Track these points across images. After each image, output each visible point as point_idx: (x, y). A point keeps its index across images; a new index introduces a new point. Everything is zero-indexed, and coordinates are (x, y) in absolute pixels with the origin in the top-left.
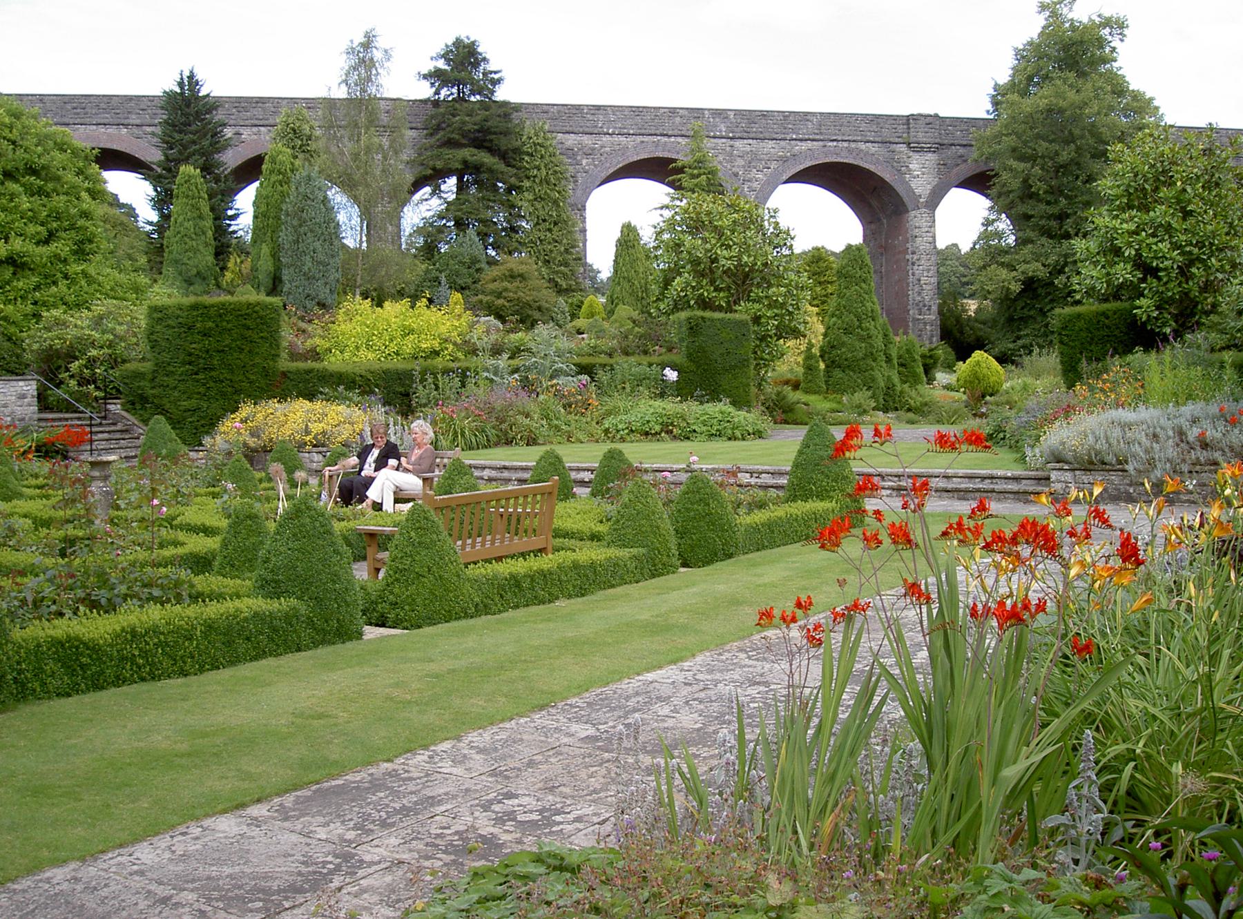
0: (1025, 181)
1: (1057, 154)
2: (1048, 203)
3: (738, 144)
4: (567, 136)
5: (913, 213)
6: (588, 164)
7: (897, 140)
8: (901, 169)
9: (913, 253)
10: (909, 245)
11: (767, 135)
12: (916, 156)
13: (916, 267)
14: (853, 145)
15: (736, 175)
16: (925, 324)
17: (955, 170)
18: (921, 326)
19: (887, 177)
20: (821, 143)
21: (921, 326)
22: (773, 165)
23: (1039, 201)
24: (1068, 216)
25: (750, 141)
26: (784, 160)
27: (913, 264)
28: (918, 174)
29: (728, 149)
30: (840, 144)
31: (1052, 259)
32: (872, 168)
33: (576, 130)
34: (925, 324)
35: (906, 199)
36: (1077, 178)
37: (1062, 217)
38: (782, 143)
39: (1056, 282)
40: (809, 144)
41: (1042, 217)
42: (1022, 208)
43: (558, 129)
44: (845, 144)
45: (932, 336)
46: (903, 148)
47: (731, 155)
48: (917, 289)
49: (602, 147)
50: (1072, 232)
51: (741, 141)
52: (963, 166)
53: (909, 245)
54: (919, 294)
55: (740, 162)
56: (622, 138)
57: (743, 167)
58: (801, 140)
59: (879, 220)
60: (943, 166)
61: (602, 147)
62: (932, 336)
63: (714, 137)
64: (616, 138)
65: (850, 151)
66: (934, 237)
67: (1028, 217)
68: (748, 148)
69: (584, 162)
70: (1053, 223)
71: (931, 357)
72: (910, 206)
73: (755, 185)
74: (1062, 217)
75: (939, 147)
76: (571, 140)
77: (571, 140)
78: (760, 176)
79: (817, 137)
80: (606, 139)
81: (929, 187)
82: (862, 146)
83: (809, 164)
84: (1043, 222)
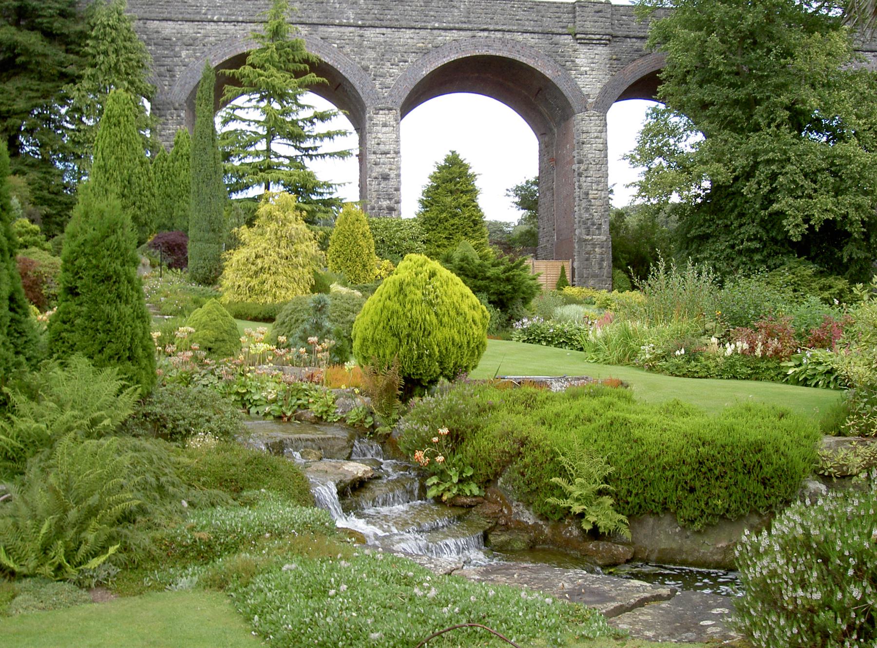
0: (701, 55)
1: (740, 17)
2: (732, 85)
3: (369, 33)
4: (164, 24)
5: (579, 116)
6: (188, 56)
7: (560, 30)
8: (565, 64)
9: (580, 162)
10: (575, 154)
11: (404, 23)
12: (583, 49)
13: (583, 179)
14: (508, 36)
15: (366, 69)
16: (594, 245)
17: (631, 66)
18: (589, 248)
19: (548, 73)
20: (469, 33)
21: (589, 248)
22: (411, 58)
23: (721, 84)
24: (758, 102)
25: (384, 30)
26: (425, 52)
27: (580, 175)
28: (587, 70)
29: (357, 39)
30: (492, 35)
31: (741, 162)
32: (531, 63)
33: (174, 17)
34: (594, 245)
35: (571, 99)
36: (769, 50)
37: (750, 104)
38: (422, 32)
39: (744, 191)
40: (455, 34)
41: (723, 105)
42: (697, 94)
43: (153, 15)
44: (499, 35)
45: (602, 260)
46: (568, 39)
47: (360, 46)
48: (584, 204)
49: (205, 36)
50: (763, 123)
51: (373, 30)
52: (639, 62)
53: (575, 154)
54: (587, 210)
55: (372, 54)
56: (230, 27)
57: (375, 60)
58: (445, 29)
59: (551, 130)
60: (616, 62)
61: (205, 36)
62: (602, 260)
63: (340, 25)
64: (222, 27)
65: (504, 42)
66: (605, 144)
67: (705, 106)
68: (381, 39)
69: (184, 54)
70: (738, 112)
71: (508, 280)
72: (575, 105)
73: (389, 81)
74: (750, 104)
75: (611, 39)
76: (168, 29)
77: (168, 29)
78: (395, 70)
79: (464, 26)
80: (210, 27)
81: (599, 85)
82: (519, 37)
83: (453, 57)
84: (724, 111)
